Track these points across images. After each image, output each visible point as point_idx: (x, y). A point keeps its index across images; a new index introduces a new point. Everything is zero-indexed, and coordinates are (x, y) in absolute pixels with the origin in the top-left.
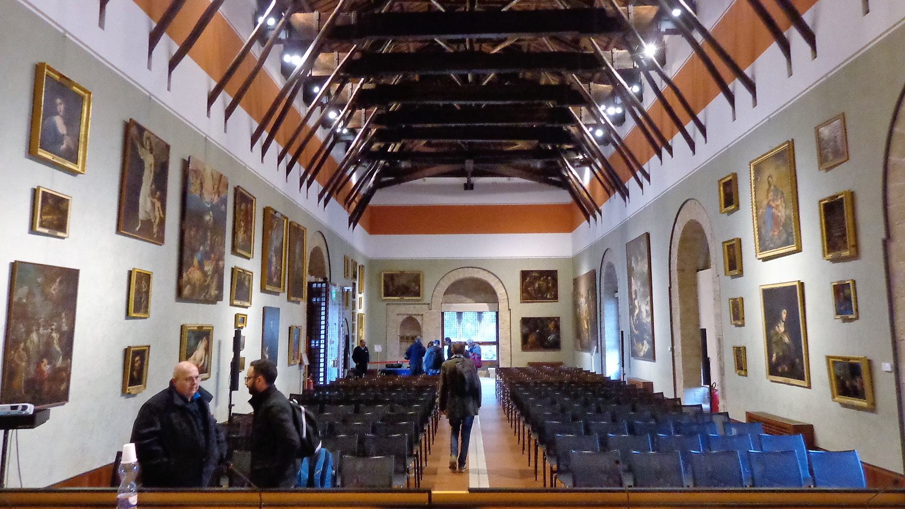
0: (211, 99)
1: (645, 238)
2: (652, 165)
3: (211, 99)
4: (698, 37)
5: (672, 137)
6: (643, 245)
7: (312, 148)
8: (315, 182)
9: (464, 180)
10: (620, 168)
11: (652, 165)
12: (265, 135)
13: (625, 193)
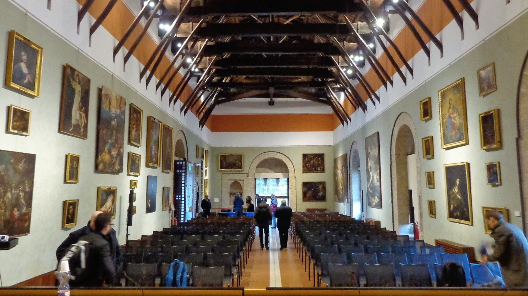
0: (116, 51)
1: (376, 135)
2: (381, 91)
3: (116, 51)
4: (409, 16)
5: (393, 75)
6: (375, 139)
7: (177, 81)
8: (179, 101)
9: (268, 100)
10: (362, 93)
11: (381, 91)
12: (148, 73)
13: (365, 108)
